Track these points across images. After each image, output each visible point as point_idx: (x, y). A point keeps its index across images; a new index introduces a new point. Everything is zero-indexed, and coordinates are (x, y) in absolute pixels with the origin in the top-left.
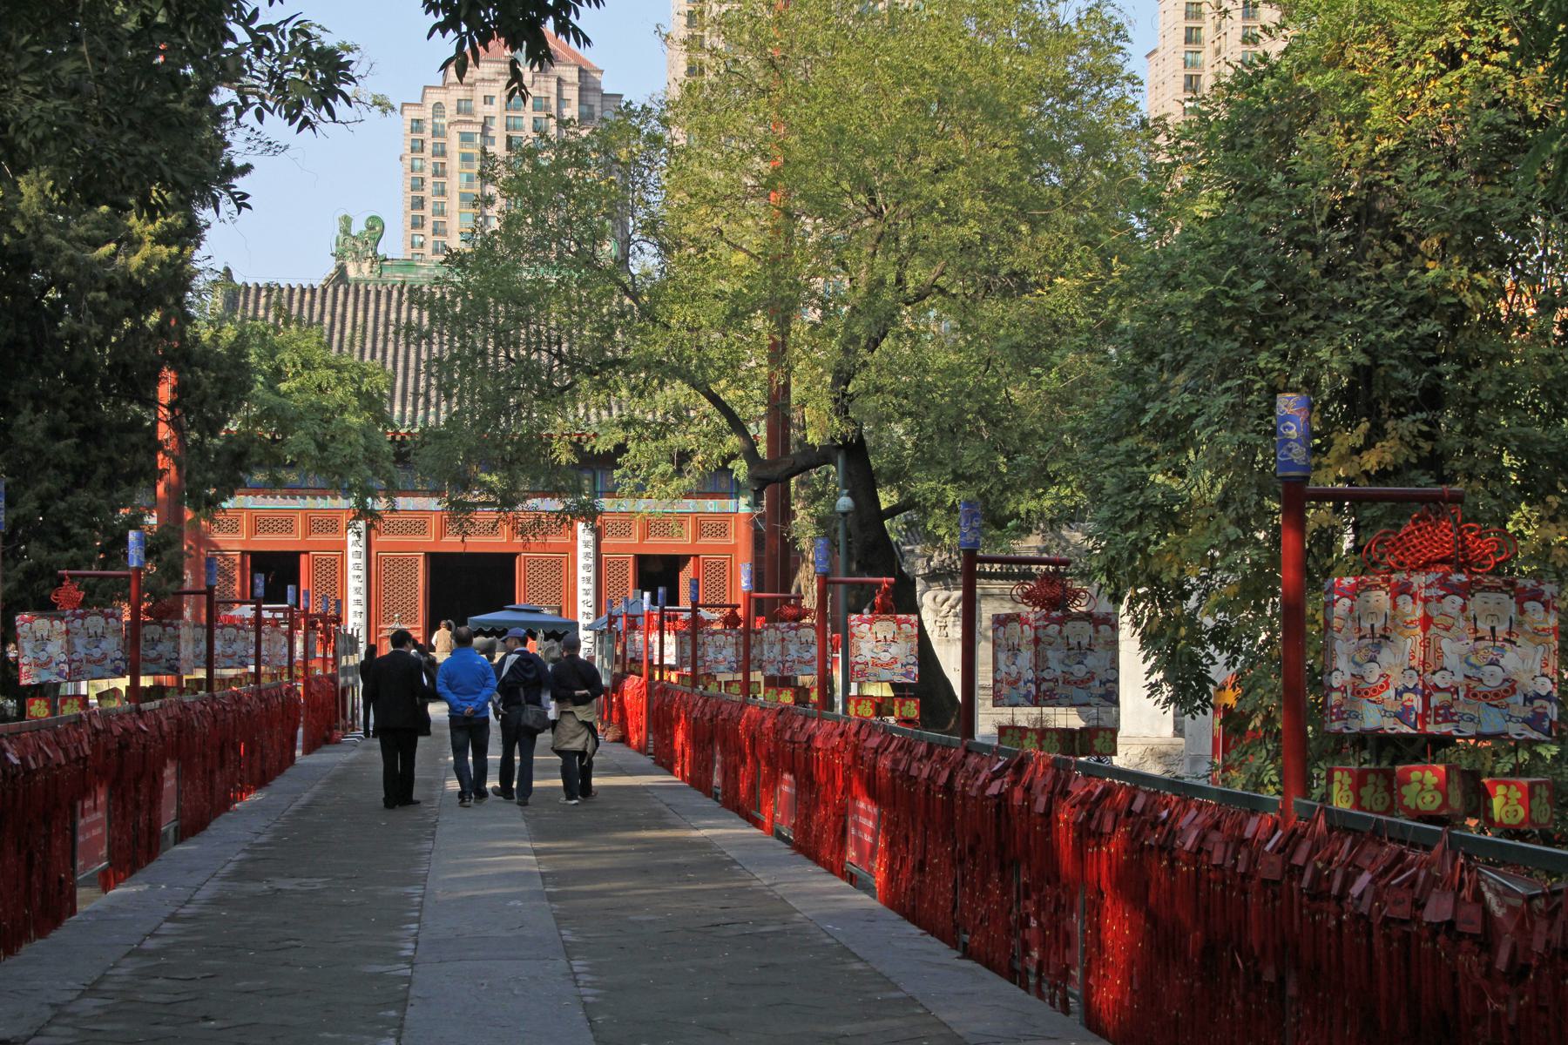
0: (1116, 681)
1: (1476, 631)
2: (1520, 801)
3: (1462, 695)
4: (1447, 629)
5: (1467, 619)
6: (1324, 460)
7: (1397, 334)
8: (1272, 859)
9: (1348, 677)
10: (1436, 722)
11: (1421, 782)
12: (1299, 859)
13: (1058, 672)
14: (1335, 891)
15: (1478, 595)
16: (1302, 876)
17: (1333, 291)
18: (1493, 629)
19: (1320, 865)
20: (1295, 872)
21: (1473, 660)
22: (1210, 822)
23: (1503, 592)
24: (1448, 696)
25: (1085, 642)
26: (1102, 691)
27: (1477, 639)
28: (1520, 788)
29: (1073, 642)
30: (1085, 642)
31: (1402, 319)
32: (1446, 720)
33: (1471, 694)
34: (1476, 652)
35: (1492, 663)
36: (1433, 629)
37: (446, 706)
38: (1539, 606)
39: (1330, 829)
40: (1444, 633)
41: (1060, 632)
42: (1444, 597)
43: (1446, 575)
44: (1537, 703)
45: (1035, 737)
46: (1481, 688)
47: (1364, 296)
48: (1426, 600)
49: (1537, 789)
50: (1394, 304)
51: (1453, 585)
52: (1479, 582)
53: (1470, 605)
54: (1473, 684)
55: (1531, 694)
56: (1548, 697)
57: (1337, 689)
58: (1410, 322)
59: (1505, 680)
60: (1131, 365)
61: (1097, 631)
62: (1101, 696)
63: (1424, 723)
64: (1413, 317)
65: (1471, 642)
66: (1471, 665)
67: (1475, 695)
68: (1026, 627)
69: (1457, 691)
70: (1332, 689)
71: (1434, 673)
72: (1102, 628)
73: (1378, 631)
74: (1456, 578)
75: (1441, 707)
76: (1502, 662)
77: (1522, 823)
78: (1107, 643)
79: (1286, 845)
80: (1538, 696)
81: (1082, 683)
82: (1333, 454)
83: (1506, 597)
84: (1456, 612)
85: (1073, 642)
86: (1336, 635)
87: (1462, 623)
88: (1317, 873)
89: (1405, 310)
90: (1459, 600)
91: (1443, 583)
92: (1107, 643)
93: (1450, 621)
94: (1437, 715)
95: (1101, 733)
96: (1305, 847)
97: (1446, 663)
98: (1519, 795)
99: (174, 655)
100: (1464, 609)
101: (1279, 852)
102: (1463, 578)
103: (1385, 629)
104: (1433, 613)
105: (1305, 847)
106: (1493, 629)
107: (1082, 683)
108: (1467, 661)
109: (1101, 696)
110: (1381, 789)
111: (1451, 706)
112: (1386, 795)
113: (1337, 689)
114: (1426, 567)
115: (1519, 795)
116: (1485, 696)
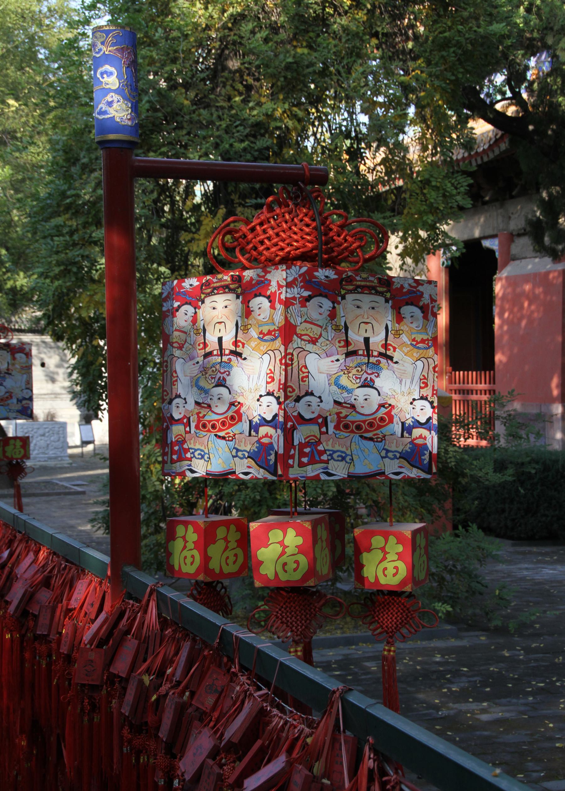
0: (31, 399)
1: (347, 343)
2: (400, 556)
3: (331, 426)
4: (314, 341)
5: (337, 329)
6: (196, 236)
7: (243, 145)
8: (92, 656)
9: (191, 405)
10: (301, 465)
11: (281, 543)
12: (121, 667)
14: (163, 734)
15: (349, 297)
16: (125, 689)
17: (199, 115)
18: (367, 340)
19: (147, 679)
20: (118, 684)
22: (40, 577)
23: (378, 293)
24: (314, 429)
26: (19, 407)
27: (349, 354)
28: (400, 539)
31: (247, 136)
32: (312, 462)
33: (343, 425)
35: (364, 385)
36: (296, 342)
38: (23, 355)
39: (164, 623)
40: (309, 347)
42: (308, 299)
43: (310, 272)
44: (24, 402)
46: (353, 417)
47: (220, 118)
48: (287, 303)
50: (241, 125)
51: (320, 283)
52: (350, 280)
54: (344, 412)
55: (409, 422)
56: (427, 425)
57: (179, 421)
58: (252, 139)
59: (381, 406)
60: (63, 167)
61: (14, 359)
62: (18, 411)
63: (287, 467)
64: (255, 136)
65: (342, 358)
66: (342, 388)
67: (346, 427)
69: (325, 423)
70: (173, 421)
71: (298, 399)
72: (18, 355)
73: (228, 345)
74: (322, 274)
75: (307, 444)
77: (403, 582)
78: (22, 368)
79: (110, 634)
82: (202, 232)
83: (381, 299)
84: (322, 319)
86: (177, 353)
87: (331, 334)
88: (143, 693)
89: (248, 130)
90: (327, 304)
91: (308, 281)
92: (22, 368)
94: (302, 454)
96: (130, 646)
98: (400, 548)
100: (333, 315)
101: (100, 645)
102: (330, 273)
104: (296, 320)
105: (130, 646)
108: (337, 384)
109: (18, 411)
110: (232, 544)
111: (319, 442)
112: (239, 551)
113: (179, 421)
114: (287, 261)
115: (400, 548)
116: (359, 427)
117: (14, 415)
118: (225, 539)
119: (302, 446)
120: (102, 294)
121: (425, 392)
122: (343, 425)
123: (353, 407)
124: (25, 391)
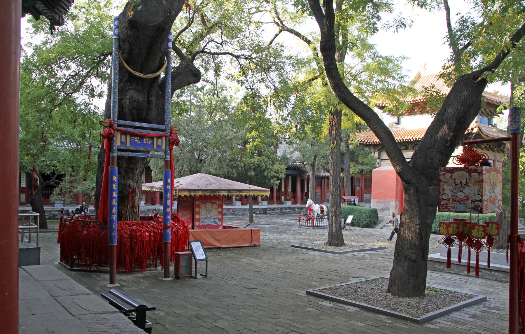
1: (455, 183)
4: (446, 183)
5: (452, 180)
9: (488, 197)
13: (450, 196)
15: (456, 173)
18: (461, 182)
21: (454, 191)
24: (446, 201)
25: (464, 181)
26: (473, 205)
27: (455, 185)
29: (458, 181)
30: (464, 181)
34: (455, 189)
35: (460, 192)
37: (199, 243)
38: (477, 174)
41: (451, 177)
44: (476, 203)
45: (445, 226)
49: (442, 225)
53: (453, 175)
61: (471, 176)
68: (499, 175)
69: (449, 200)
72: (473, 174)
76: (464, 191)
80: (477, 201)
81: (461, 201)
85: (458, 181)
87: (451, 181)
93: (447, 180)
94: (443, 206)
95: (477, 227)
97: (446, 192)
99: (478, 198)
103: (466, 183)
106: (461, 182)
107: (461, 201)
117: (469, 210)
118: (478, 229)
119: (443, 205)
120: (92, 177)
121: (479, 193)
122: (454, 200)
123: (457, 197)
124: (477, 196)
